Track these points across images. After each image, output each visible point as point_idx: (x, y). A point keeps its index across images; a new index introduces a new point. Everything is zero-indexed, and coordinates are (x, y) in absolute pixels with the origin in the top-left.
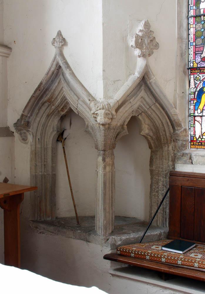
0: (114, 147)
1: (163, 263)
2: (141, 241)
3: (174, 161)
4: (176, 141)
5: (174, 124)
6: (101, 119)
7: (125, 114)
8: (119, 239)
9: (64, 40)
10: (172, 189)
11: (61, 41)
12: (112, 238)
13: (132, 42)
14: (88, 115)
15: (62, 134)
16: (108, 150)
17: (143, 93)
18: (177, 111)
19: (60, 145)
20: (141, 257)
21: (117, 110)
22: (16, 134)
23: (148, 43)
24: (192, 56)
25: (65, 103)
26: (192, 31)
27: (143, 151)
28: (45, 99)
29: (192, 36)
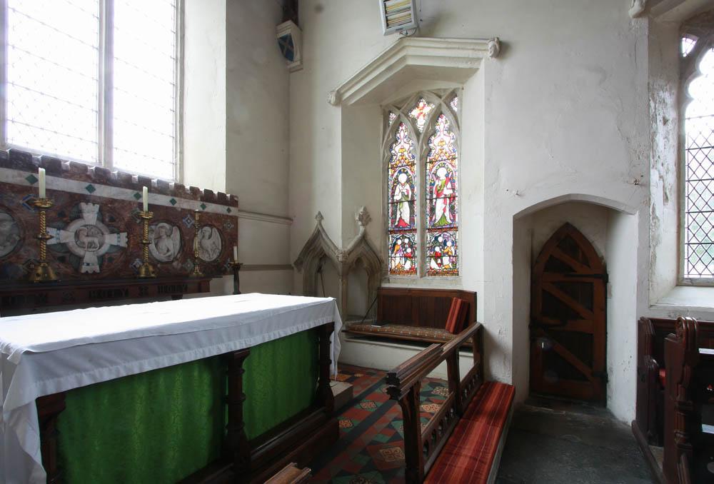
0: (347, 274)
1: (417, 337)
2: (362, 323)
3: (380, 283)
4: (381, 270)
5: (380, 262)
6: (340, 259)
7: (353, 257)
8: (349, 323)
9: (322, 216)
10: (378, 296)
11: (320, 217)
12: (346, 323)
13: (357, 218)
14: (334, 257)
15: (320, 268)
16: (345, 275)
17: (363, 245)
18: (382, 254)
19: (319, 275)
20: (361, 330)
21: (349, 254)
22: (295, 269)
23: (366, 218)
24: (390, 225)
25: (322, 251)
26: (390, 211)
27: (365, 277)
28: (311, 248)
29: (390, 213)
